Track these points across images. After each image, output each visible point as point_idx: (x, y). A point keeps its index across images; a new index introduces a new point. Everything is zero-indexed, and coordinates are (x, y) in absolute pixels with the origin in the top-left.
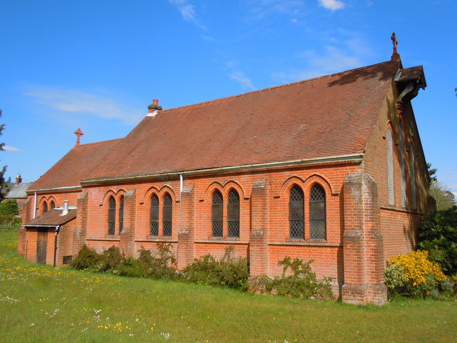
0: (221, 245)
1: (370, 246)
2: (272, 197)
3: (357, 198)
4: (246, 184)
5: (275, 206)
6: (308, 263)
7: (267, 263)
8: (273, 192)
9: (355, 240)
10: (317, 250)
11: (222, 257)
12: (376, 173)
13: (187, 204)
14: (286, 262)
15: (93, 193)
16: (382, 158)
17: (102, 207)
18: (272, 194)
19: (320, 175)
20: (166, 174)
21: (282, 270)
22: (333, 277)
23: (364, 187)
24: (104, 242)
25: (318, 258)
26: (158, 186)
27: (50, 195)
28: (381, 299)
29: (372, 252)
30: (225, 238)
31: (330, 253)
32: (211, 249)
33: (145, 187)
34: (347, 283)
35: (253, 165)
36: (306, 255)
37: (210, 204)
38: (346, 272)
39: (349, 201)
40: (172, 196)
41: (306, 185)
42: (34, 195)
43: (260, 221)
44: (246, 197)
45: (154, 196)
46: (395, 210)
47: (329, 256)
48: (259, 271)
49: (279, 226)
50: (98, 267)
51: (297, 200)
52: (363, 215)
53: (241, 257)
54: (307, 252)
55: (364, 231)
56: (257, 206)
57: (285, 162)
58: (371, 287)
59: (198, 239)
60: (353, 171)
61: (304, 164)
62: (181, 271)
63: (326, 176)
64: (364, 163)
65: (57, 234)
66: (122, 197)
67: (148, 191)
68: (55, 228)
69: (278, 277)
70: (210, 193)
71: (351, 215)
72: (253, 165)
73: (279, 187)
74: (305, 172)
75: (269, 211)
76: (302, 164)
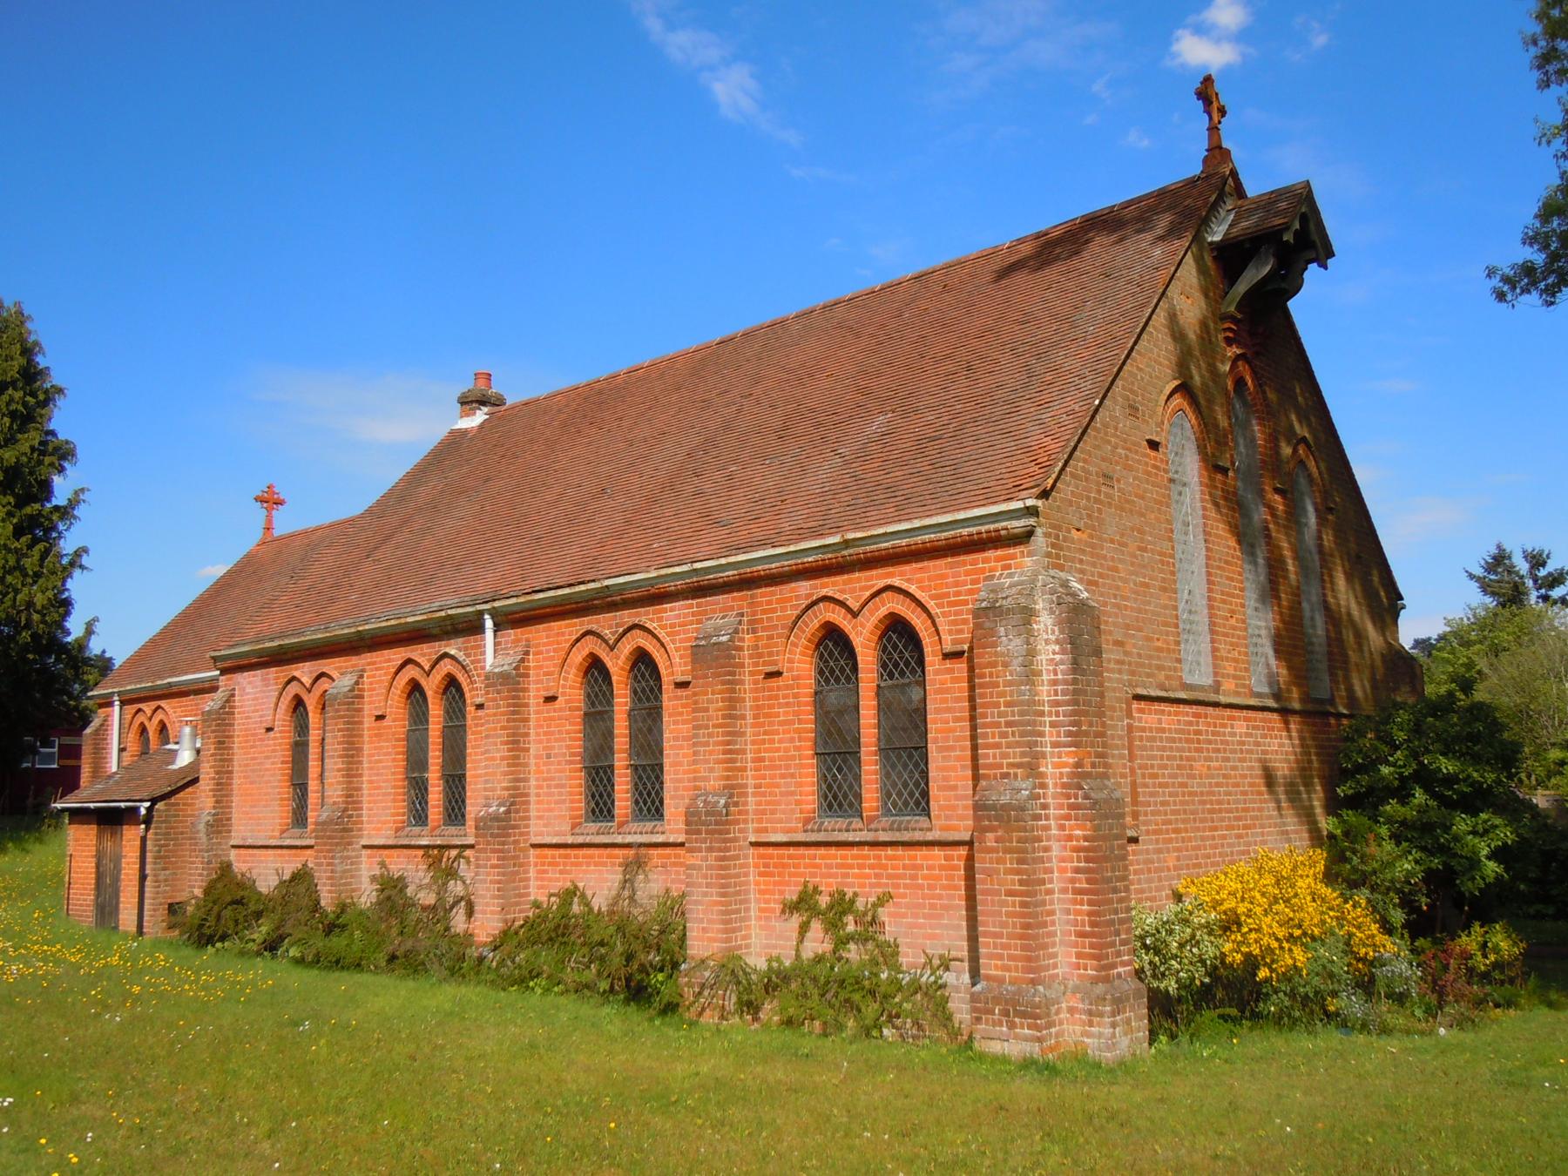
0: (608, 851)
1: (1070, 838)
2: (759, 673)
3: (1015, 662)
4: (678, 633)
5: (770, 707)
6: (874, 905)
7: (747, 910)
8: (760, 656)
9: (1009, 816)
10: (903, 858)
11: (614, 893)
12: (1116, 570)
13: (503, 714)
14: (803, 904)
15: (249, 690)
16: (1143, 515)
17: (271, 734)
18: (757, 664)
19: (905, 586)
20: (443, 614)
21: (795, 935)
22: (954, 954)
23: (1046, 624)
24: (279, 851)
25: (906, 886)
26: (423, 655)
27: (154, 704)
28: (1119, 1036)
29: (1079, 861)
30: (621, 825)
31: (942, 868)
32: (580, 864)
33: (389, 661)
34: (988, 978)
35: (698, 565)
36: (868, 876)
37: (578, 709)
38: (986, 934)
39: (991, 675)
40: (466, 689)
41: (862, 625)
42: (111, 704)
43: (719, 762)
44: (680, 679)
45: (595, 669)
46: (1216, 705)
47: (938, 878)
48: (715, 940)
49: (783, 776)
50: (255, 936)
51: (837, 680)
52: (1043, 724)
53: (667, 891)
54: (872, 867)
55: (1050, 782)
56: (707, 710)
57: (792, 548)
58: (1076, 989)
59: (541, 834)
60: (1008, 567)
61: (851, 551)
62: (485, 944)
63: (922, 589)
64: (1047, 535)
65: (147, 829)
66: (451, 683)
67: (397, 673)
68: (137, 809)
69: (778, 959)
70: (574, 671)
71: (998, 725)
72: (698, 565)
73: (779, 636)
74: (859, 580)
75: (754, 725)
76: (845, 553)
